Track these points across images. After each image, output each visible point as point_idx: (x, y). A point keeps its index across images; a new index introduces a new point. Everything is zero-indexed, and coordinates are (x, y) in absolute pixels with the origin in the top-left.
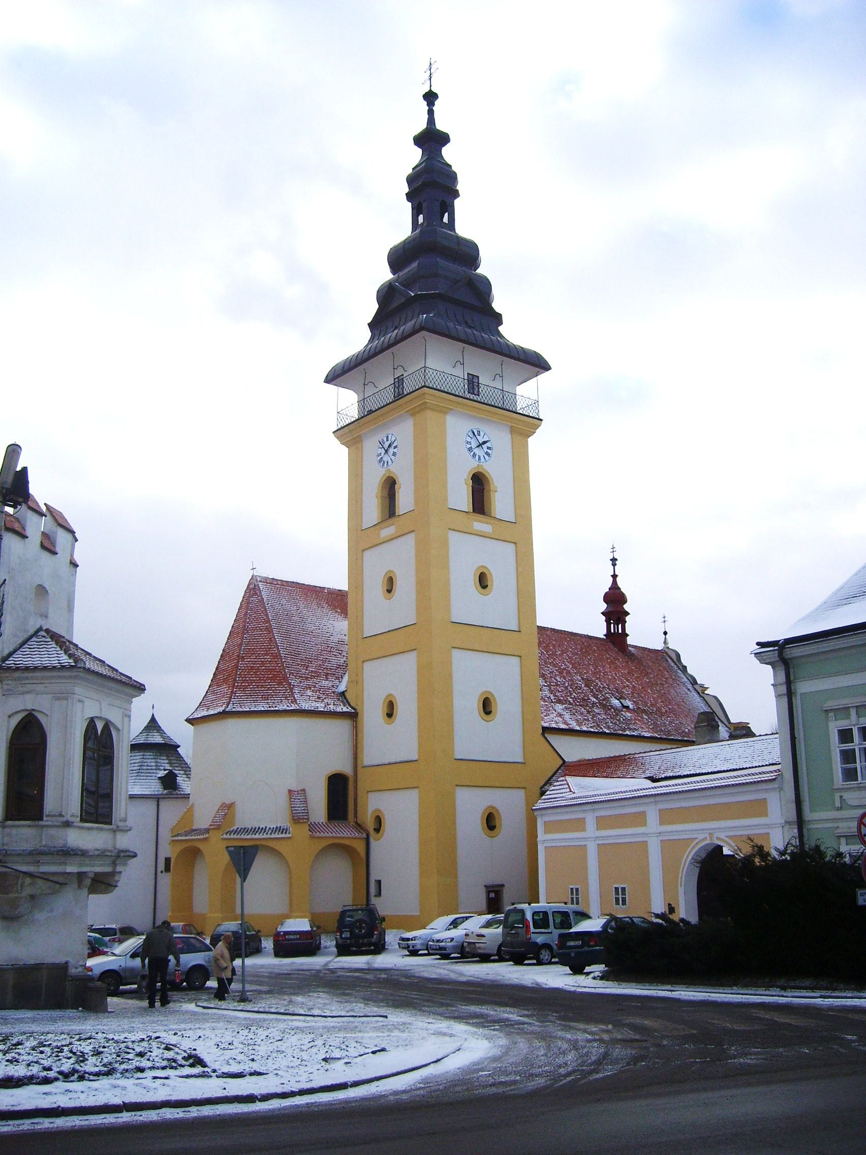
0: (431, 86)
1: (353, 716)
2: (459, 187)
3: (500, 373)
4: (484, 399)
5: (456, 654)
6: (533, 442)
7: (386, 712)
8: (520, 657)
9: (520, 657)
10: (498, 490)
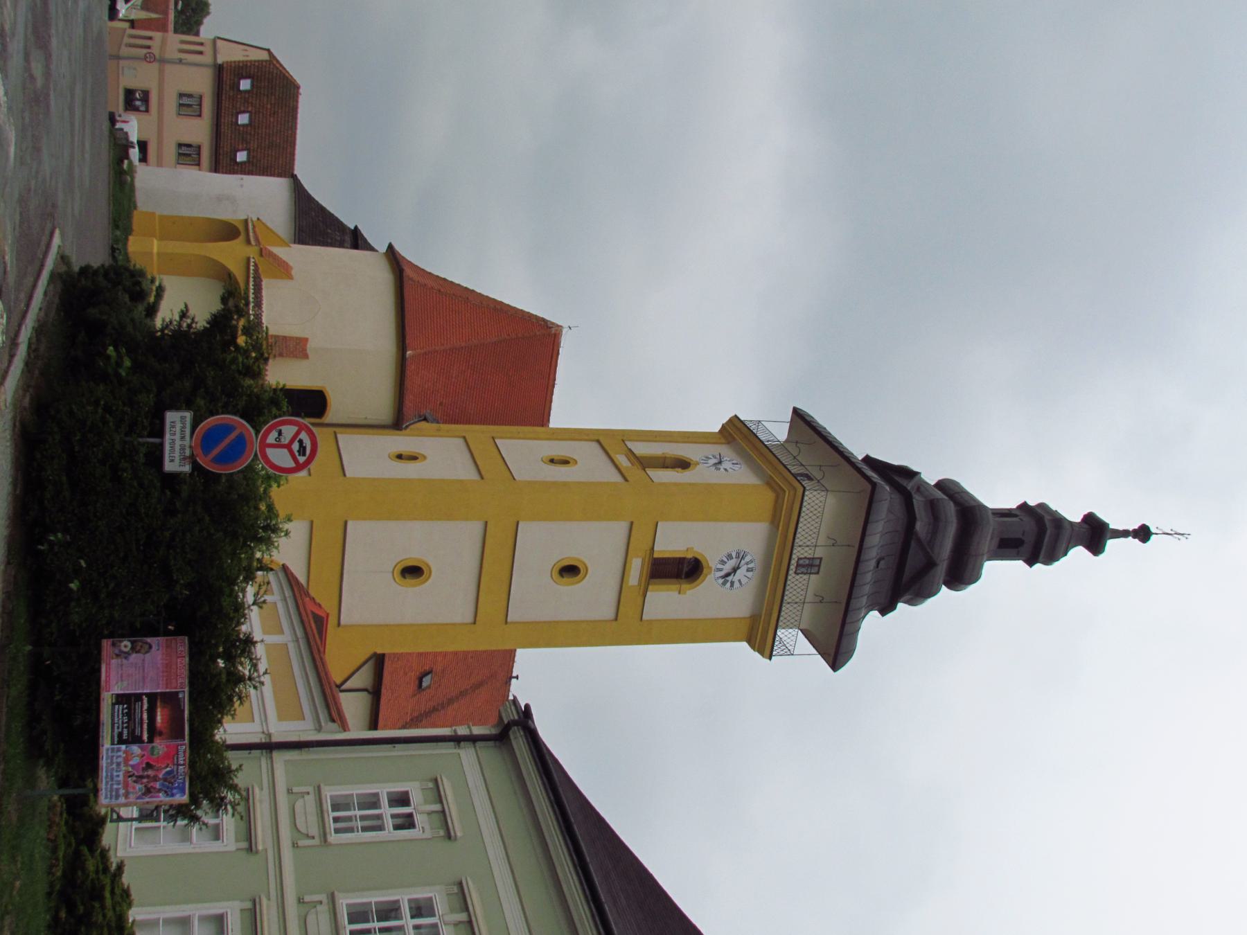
0: (1157, 534)
1: (398, 423)
2: (1038, 566)
3: (825, 600)
4: (791, 591)
5: (475, 528)
6: (743, 647)
7: (403, 453)
8: (475, 623)
9: (475, 623)
10: (680, 596)
